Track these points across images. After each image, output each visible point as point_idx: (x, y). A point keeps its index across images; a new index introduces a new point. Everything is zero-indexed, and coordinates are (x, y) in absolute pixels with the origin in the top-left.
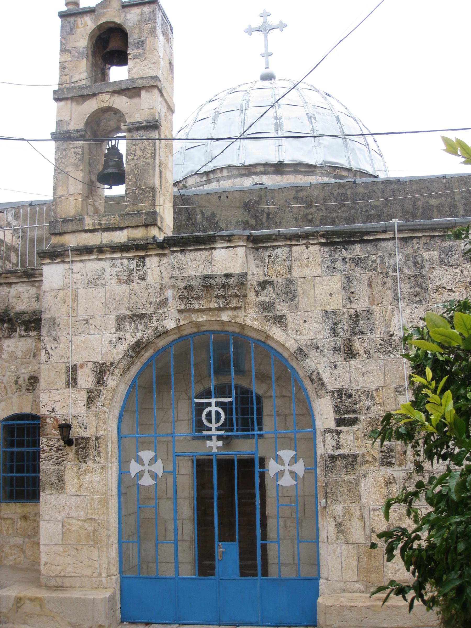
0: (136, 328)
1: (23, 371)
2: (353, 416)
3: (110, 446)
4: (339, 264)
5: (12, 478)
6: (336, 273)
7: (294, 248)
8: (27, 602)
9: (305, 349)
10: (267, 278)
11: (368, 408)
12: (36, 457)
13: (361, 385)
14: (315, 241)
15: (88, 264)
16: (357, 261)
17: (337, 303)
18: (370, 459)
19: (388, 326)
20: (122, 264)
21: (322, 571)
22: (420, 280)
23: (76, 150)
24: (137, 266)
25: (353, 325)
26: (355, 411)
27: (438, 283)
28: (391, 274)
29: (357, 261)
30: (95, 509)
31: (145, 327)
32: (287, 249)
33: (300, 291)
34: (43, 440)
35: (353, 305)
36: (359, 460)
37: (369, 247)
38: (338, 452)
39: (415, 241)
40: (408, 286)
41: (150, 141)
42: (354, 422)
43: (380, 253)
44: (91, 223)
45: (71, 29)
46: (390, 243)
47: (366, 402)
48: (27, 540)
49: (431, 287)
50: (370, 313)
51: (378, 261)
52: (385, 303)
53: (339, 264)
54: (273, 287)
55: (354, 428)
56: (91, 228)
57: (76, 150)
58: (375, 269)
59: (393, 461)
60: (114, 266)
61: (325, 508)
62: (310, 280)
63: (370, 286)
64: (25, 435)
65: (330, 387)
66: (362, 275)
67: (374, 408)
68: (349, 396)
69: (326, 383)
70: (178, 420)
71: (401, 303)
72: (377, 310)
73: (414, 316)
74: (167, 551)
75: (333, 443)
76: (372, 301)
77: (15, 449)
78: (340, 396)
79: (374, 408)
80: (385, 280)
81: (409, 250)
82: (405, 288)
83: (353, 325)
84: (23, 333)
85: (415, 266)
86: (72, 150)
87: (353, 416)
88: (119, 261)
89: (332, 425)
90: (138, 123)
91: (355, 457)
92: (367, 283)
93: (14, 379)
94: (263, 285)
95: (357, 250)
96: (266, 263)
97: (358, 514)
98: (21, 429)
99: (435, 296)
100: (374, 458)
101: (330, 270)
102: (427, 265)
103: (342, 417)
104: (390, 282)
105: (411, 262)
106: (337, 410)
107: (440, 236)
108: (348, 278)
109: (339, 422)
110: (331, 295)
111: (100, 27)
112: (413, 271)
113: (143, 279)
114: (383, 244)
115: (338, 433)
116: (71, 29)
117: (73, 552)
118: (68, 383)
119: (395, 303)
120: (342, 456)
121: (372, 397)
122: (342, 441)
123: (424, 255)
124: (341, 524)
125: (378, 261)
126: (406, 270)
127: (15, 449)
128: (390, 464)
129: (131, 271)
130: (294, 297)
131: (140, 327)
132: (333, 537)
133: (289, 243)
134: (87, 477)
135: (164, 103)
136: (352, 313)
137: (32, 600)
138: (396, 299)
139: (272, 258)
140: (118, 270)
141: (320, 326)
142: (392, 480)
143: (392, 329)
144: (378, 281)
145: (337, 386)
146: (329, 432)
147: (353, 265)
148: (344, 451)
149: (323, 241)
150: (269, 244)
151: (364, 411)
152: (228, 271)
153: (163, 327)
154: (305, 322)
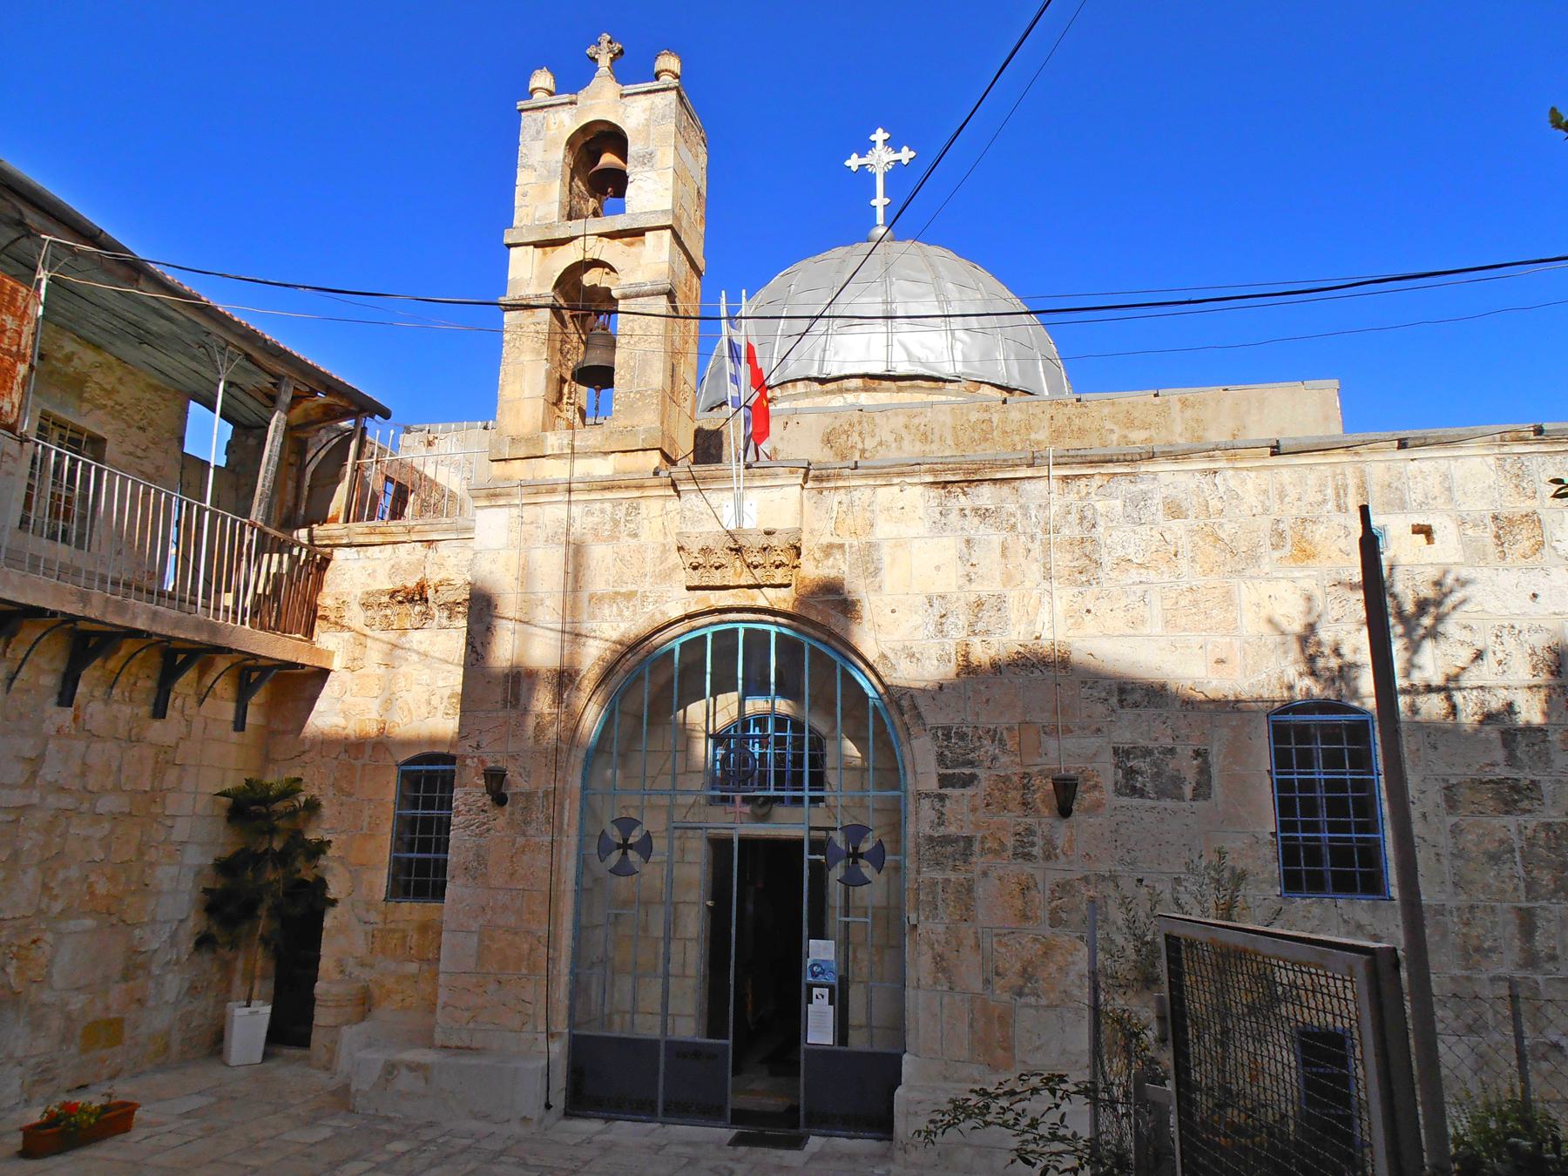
0: (620, 614)
1: (441, 684)
2: (967, 771)
3: (567, 806)
4: (954, 517)
5: (410, 860)
6: (948, 533)
7: (879, 490)
8: (404, 1071)
9: (891, 656)
10: (837, 540)
11: (994, 758)
12: (445, 825)
13: (982, 719)
14: (916, 480)
15: (548, 508)
16: (983, 514)
17: (948, 581)
18: (996, 846)
19: (1032, 623)
20: (602, 511)
21: (909, 1039)
22: (1089, 547)
23: (538, 328)
24: (628, 514)
25: (972, 619)
26: (971, 763)
27: (1120, 553)
28: (1039, 536)
29: (983, 514)
30: (533, 912)
31: (634, 613)
32: (868, 491)
33: (887, 560)
34: (458, 793)
35: (974, 586)
36: (976, 847)
37: (1005, 490)
38: (942, 831)
39: (1084, 481)
40: (1069, 557)
41: (799, 384)
42: (969, 780)
43: (1022, 501)
44: (556, 444)
45: (538, 132)
46: (1043, 484)
47: (989, 747)
48: (425, 967)
49: (1107, 560)
50: (1001, 599)
51: (1019, 515)
52: (1027, 584)
53: (954, 517)
54: (844, 553)
55: (969, 791)
56: (556, 452)
57: (538, 328)
58: (1013, 527)
59: (1035, 851)
60: (590, 513)
61: (915, 926)
62: (899, 543)
63: (1003, 555)
64: (736, 845)
65: (931, 720)
66: (991, 537)
67: (1004, 759)
68: (962, 736)
69: (924, 714)
70: (686, 772)
71: (1055, 584)
72: (1013, 596)
73: (1076, 606)
74: (652, 993)
75: (933, 815)
76: (1008, 579)
77: (420, 812)
78: (947, 737)
79: (1004, 759)
80: (1030, 546)
81: (1072, 497)
82: (1062, 560)
83: (972, 619)
84: (445, 622)
85: (1081, 524)
86: (532, 328)
87: (967, 771)
88: (598, 506)
89: (932, 784)
90: (637, 285)
91: (969, 840)
92: (999, 551)
93: (425, 696)
94: (829, 550)
95: (985, 495)
96: (834, 515)
97: (972, 942)
98: (431, 778)
99: (1113, 575)
100: (1002, 844)
101: (940, 524)
102: (1101, 522)
103: (950, 771)
104: (1036, 548)
105: (1074, 518)
106: (941, 759)
107: (1127, 474)
108: (968, 541)
109: (944, 781)
110: (938, 568)
111: (585, 129)
112: (1077, 532)
113: (636, 535)
114: (1027, 485)
115: (942, 798)
116: (538, 132)
117: (492, 987)
118: (505, 700)
119: (1046, 585)
120: (947, 840)
121: (1000, 740)
122: (948, 815)
123: (1098, 505)
124: (942, 959)
125: (1019, 515)
126: (1066, 531)
127: (420, 812)
128: (1028, 857)
129: (616, 523)
130: (877, 571)
131: (626, 613)
132: (926, 980)
133: (871, 482)
134: (525, 858)
135: (683, 257)
136: (973, 598)
137: (414, 1068)
138: (1048, 577)
139: (844, 507)
140: (596, 520)
141: (917, 619)
142: (1032, 885)
143: (1038, 628)
144: (1018, 544)
145: (942, 720)
146: (927, 795)
147: (976, 520)
148: (952, 830)
149: (930, 479)
150: (840, 483)
151: (987, 764)
152: (770, 526)
153: (663, 613)
154: (893, 611)
